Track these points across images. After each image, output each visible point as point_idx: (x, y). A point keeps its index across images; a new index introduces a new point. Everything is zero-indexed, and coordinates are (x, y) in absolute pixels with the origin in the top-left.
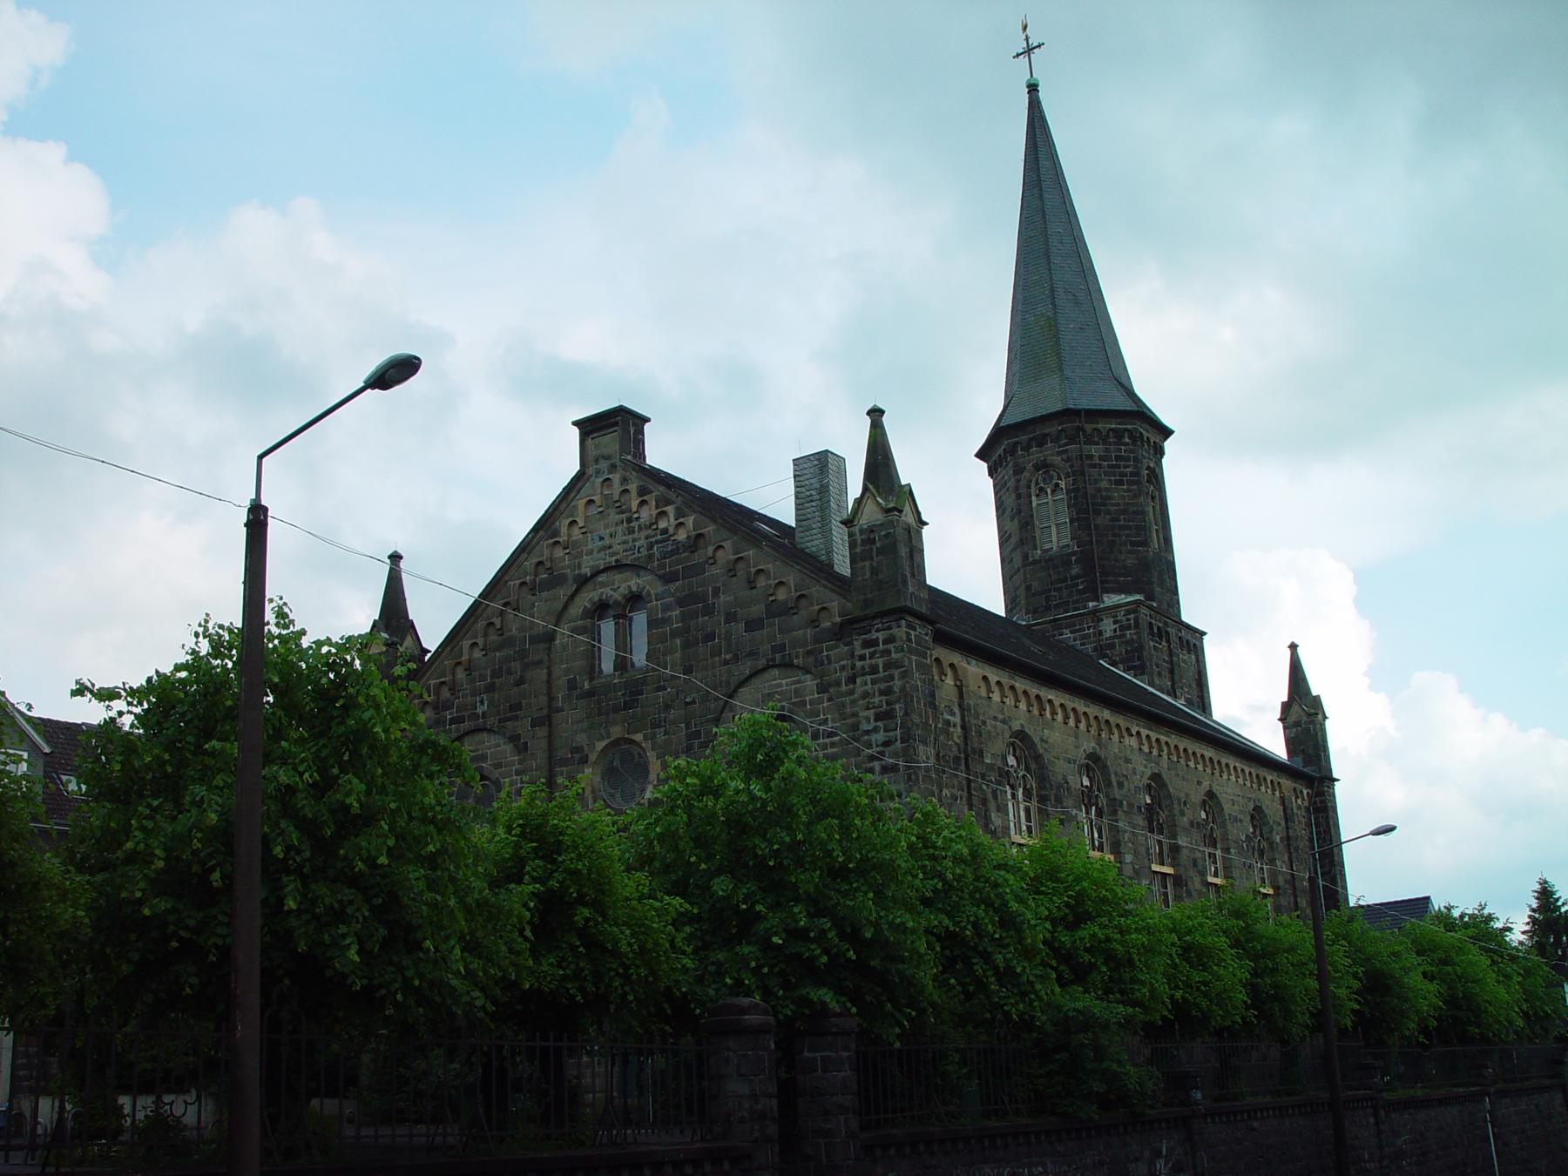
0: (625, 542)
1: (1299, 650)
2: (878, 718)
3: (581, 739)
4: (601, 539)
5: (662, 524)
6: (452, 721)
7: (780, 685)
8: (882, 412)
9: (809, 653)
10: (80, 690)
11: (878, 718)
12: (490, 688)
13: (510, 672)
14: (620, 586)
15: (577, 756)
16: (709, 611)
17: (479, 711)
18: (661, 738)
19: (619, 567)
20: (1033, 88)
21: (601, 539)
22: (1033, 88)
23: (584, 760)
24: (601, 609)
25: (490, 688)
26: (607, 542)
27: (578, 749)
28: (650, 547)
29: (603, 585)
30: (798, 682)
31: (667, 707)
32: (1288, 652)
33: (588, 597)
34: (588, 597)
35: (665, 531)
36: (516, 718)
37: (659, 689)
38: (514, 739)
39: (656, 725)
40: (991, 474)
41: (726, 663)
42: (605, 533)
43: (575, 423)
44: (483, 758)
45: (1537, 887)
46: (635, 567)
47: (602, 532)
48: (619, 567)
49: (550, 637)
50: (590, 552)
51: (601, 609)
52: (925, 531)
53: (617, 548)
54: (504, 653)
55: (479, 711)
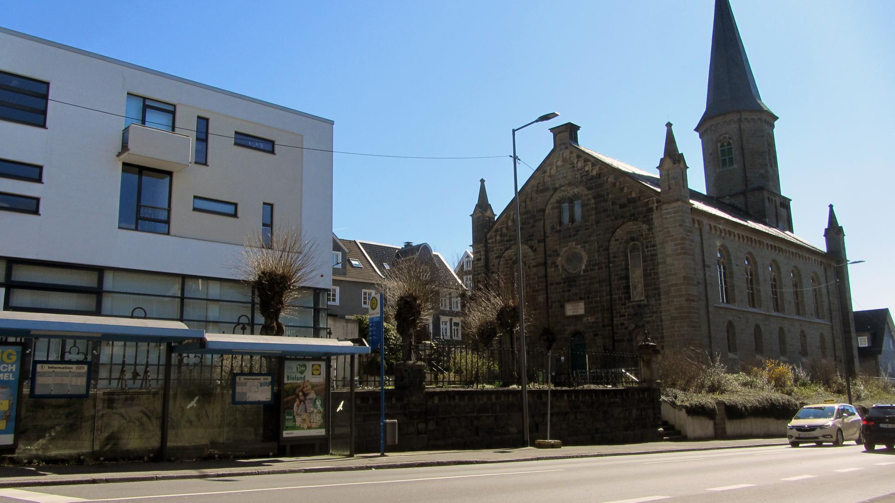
3: (557, 247)
6: (507, 241)
16: (606, 201)
18: (587, 247)
19: (570, 184)
28: (582, 177)
29: (564, 191)
39: (586, 242)
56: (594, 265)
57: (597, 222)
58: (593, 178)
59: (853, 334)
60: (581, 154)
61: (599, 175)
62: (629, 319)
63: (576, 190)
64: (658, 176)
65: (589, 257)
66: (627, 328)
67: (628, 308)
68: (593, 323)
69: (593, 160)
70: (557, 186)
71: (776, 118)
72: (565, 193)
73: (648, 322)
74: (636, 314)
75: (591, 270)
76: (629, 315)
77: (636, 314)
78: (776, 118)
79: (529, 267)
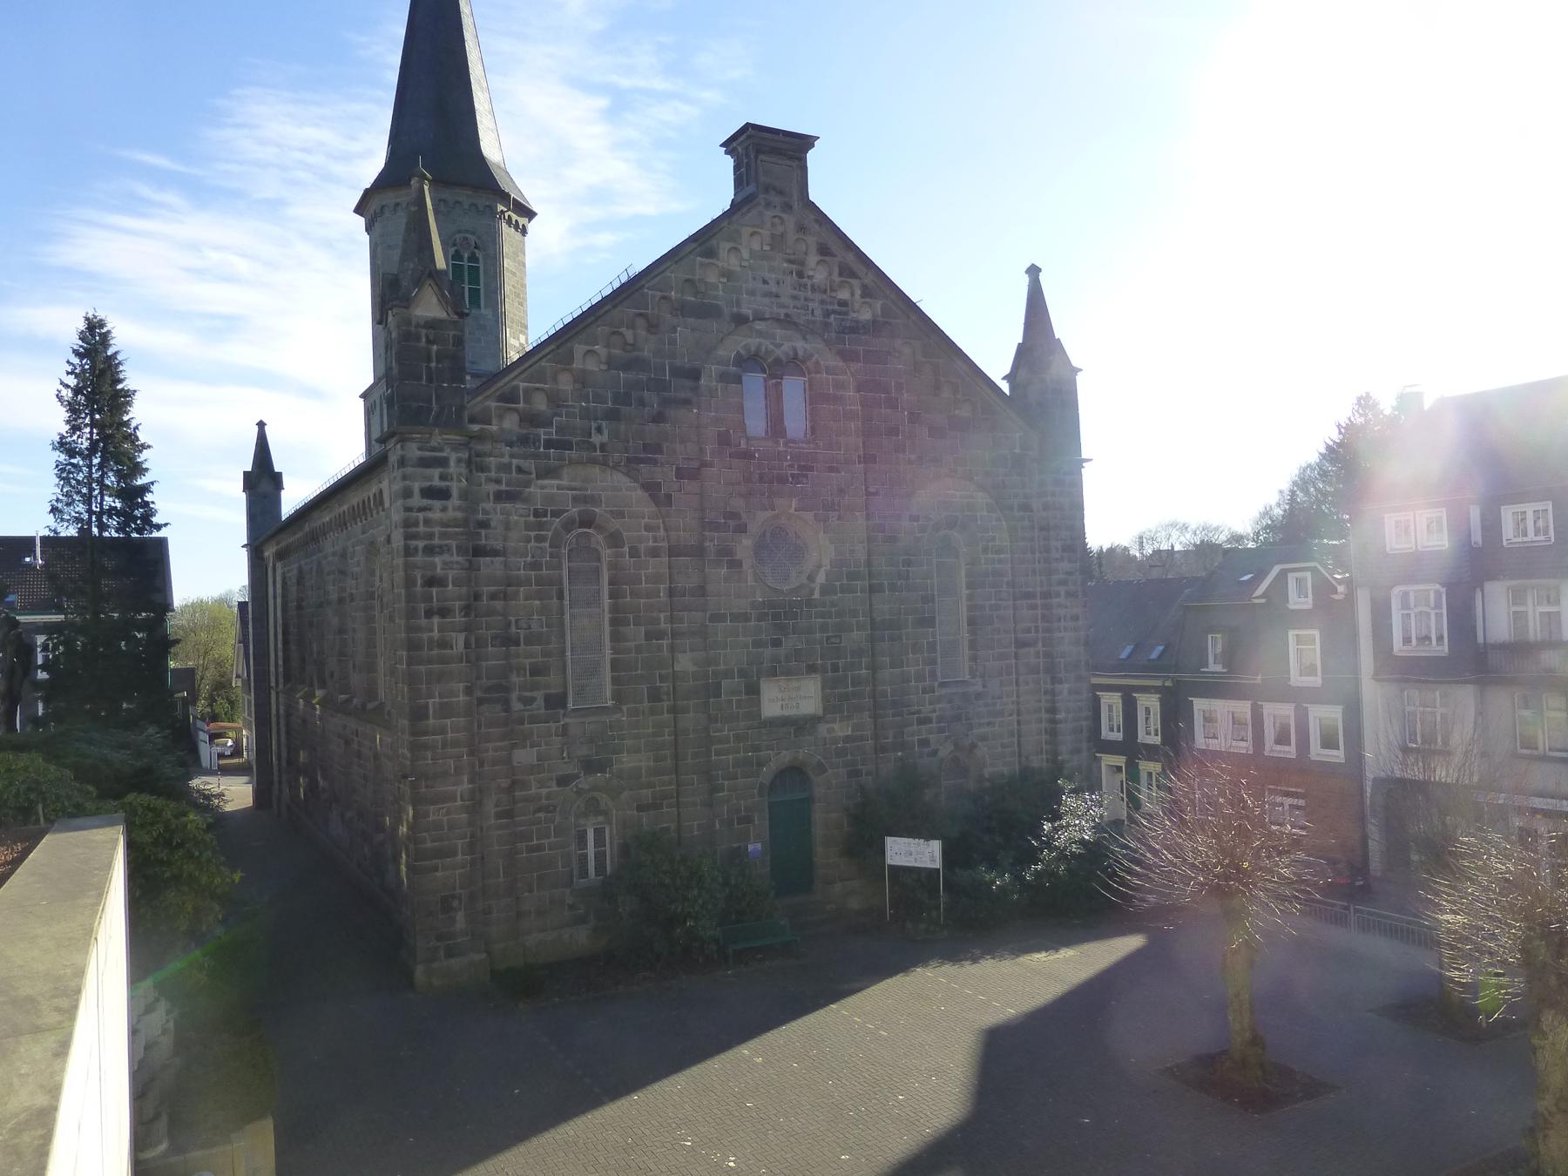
0: (795, 298)
1: (1042, 277)
2: (1064, 550)
3: (738, 504)
4: (765, 282)
5: (844, 295)
6: (549, 444)
8: (794, 147)
11: (1064, 550)
13: (642, 403)
15: (731, 523)
17: (596, 439)
19: (787, 322)
21: (765, 282)
23: (742, 529)
24: (750, 361)
25: (613, 416)
27: (734, 515)
28: (827, 314)
29: (760, 334)
31: (841, 491)
33: (742, 342)
34: (742, 342)
35: (843, 303)
36: (654, 462)
37: (831, 469)
38: (651, 488)
42: (771, 277)
44: (593, 500)
45: (82, 326)
47: (767, 275)
49: (695, 375)
50: (752, 293)
51: (750, 361)
52: (1080, 378)
53: (784, 300)
54: (631, 376)
55: (596, 439)
56: (853, 576)
57: (868, 459)
60: (835, 246)
62: (941, 730)
66: (935, 753)
68: (847, 739)
69: (869, 280)
70: (747, 311)
71: (804, 143)
72: (767, 344)
73: (984, 738)
78: (804, 143)
79: (634, 553)
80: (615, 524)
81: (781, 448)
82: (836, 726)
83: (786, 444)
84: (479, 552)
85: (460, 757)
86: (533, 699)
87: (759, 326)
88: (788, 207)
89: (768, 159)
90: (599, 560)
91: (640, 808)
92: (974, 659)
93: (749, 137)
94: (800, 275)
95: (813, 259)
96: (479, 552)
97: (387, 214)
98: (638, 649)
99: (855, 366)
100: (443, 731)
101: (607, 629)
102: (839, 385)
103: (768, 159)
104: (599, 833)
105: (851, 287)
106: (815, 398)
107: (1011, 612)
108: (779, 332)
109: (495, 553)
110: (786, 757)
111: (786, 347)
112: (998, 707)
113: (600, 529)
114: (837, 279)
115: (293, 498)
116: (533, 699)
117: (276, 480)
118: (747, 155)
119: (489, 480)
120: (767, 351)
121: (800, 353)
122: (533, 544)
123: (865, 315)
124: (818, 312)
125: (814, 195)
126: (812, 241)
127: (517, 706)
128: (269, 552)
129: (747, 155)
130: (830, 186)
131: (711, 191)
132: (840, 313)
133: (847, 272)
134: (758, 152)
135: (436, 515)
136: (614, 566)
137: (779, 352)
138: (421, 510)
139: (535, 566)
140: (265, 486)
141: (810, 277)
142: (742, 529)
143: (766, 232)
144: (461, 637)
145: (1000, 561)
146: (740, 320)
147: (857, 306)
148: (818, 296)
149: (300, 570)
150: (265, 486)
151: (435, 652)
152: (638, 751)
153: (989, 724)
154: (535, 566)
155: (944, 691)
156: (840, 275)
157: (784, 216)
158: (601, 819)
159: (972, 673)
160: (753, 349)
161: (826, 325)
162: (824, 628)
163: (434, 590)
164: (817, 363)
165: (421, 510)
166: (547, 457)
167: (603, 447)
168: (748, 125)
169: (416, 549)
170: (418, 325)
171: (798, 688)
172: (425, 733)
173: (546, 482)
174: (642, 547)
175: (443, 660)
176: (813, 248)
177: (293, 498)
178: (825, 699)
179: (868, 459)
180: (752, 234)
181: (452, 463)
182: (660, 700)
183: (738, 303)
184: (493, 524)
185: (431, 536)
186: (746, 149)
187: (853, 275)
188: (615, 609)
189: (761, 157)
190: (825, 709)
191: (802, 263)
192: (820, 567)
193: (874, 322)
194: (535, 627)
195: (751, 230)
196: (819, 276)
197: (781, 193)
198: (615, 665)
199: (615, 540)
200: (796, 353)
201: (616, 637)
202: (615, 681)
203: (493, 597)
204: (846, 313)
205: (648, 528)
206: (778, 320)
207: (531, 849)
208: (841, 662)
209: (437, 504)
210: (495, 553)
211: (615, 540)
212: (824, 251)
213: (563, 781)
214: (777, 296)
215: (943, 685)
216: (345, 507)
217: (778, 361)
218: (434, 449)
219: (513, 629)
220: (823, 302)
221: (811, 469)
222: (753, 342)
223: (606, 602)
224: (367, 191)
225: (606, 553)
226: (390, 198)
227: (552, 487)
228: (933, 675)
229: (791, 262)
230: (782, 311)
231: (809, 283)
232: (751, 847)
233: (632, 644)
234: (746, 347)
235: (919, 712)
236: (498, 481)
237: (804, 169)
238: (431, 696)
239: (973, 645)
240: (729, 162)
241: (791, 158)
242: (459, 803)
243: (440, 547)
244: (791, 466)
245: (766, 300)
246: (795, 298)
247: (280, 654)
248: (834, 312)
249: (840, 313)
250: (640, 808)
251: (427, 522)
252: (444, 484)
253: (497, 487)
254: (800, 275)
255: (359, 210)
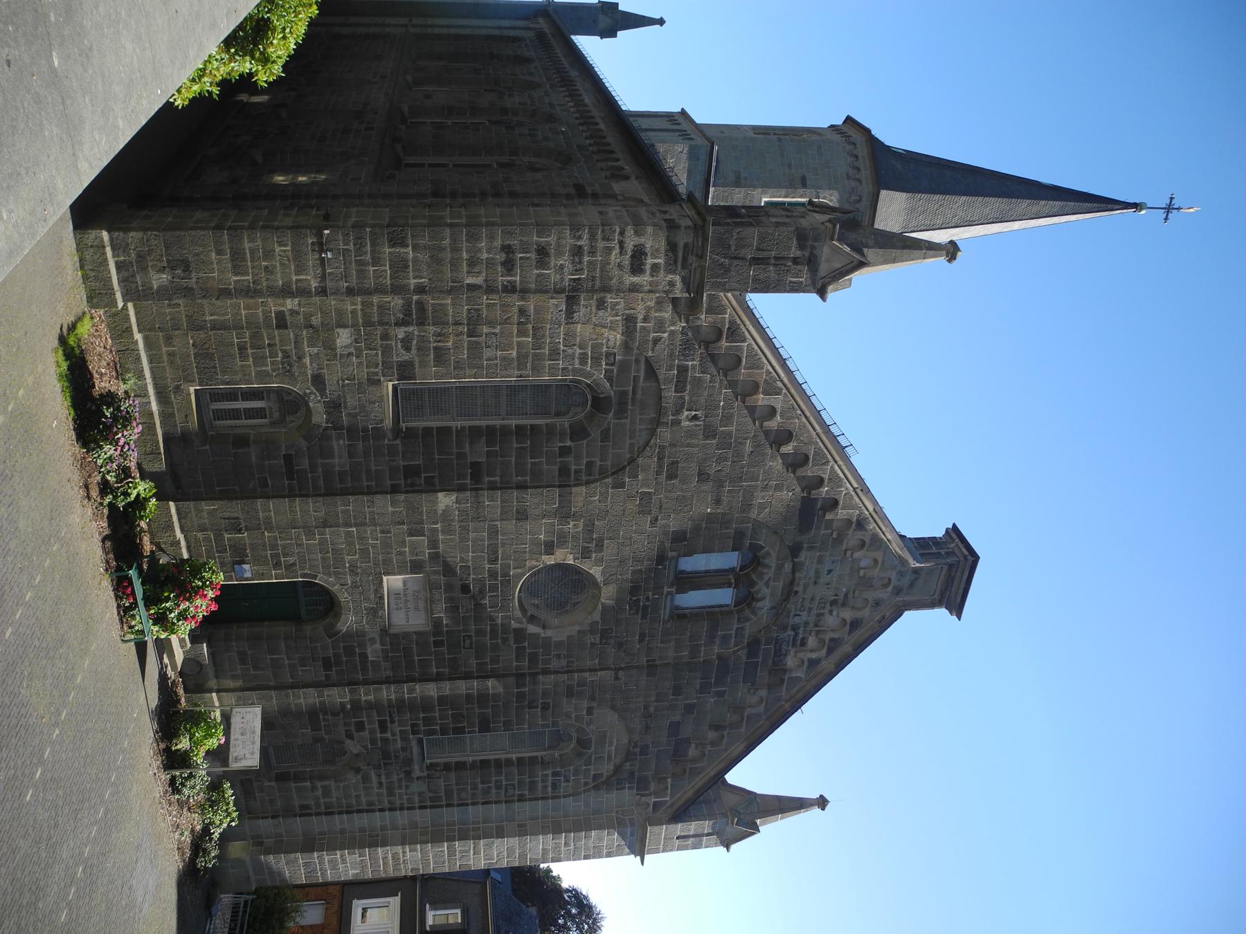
1: (816, 811)
3: (610, 550)
5: (812, 642)
6: (683, 370)
7: (611, 744)
8: (952, 596)
9: (632, 774)
10: (951, 251)
12: (709, 432)
14: (767, 593)
16: (704, 689)
18: (589, 639)
19: (789, 591)
20: (1136, 206)
21: (830, 571)
22: (1136, 206)
26: (824, 579)
27: (600, 547)
28: (795, 628)
29: (780, 567)
30: (609, 758)
31: (620, 645)
32: (658, 17)
35: (803, 643)
37: (642, 636)
39: (605, 634)
40: (832, 126)
41: (646, 707)
43: (954, 525)
46: (779, 610)
48: (789, 591)
56: (533, 659)
57: (651, 668)
58: (779, 654)
59: (274, 699)
60: (859, 634)
61: (778, 671)
62: (373, 741)
63: (765, 605)
64: (732, 777)
65: (559, 645)
66: (350, 737)
67: (405, 739)
68: (364, 656)
69: (827, 665)
70: (803, 556)
71: (957, 609)
72: (769, 574)
73: (366, 779)
74: (386, 755)
75: (520, 652)
76: (385, 740)
77: (386, 755)
78: (957, 609)
79: (564, 451)
80: (595, 434)
81: (666, 589)
82: (378, 646)
83: (669, 593)
84: (572, 301)
85: (346, 277)
86: (408, 349)
87: (788, 567)
88: (898, 591)
89: (946, 571)
90: (558, 414)
91: (288, 458)
92: (447, 767)
93: (965, 558)
94: (833, 603)
95: (847, 615)
96: (572, 301)
97: (848, 147)
98: (461, 456)
99: (743, 654)
100: (376, 261)
101: (483, 423)
102: (725, 639)
103: (946, 571)
104: (259, 413)
105: (819, 650)
106: (713, 615)
107: (493, 799)
108: (780, 584)
109: (570, 313)
110: (344, 597)
111: (766, 591)
112: (397, 791)
113: (590, 417)
114: (827, 637)
115: (588, 45)
116: (408, 349)
117: (609, 33)
118: (948, 554)
119: (648, 309)
120: (762, 574)
121: (759, 604)
122: (578, 351)
123: (790, 661)
124: (797, 620)
125: (910, 617)
126: (866, 613)
127: (401, 333)
128: (542, 23)
129: (948, 554)
130: (919, 627)
131: (912, 513)
132: (794, 640)
133: (834, 645)
134: (951, 566)
135: (614, 257)
136: (551, 429)
137: (761, 584)
138: (621, 243)
139: (554, 354)
140: (604, 21)
141: (831, 612)
142: (585, 554)
143: (876, 572)
144: (479, 280)
145: (545, 787)
146: (795, 550)
147: (801, 655)
148: (812, 620)
149: (528, 60)
150: (604, 21)
151: (465, 256)
152: (351, 455)
153: (380, 784)
154: (554, 354)
155: (414, 743)
156: (832, 640)
157: (890, 588)
158: (276, 415)
159: (431, 767)
160: (766, 561)
161: (785, 628)
162: (480, 633)
163: (533, 256)
164: (747, 620)
165: (621, 243)
166: (671, 368)
167: (677, 423)
168: (976, 558)
169: (580, 238)
170: (813, 248)
171: (417, 609)
172: (373, 244)
173: (643, 366)
174: (570, 459)
175: (455, 264)
176: (858, 615)
177: (588, 45)
178: (406, 635)
179: (651, 668)
180: (876, 561)
181: (656, 261)
182: (406, 478)
183: (811, 548)
184: (601, 313)
185: (592, 252)
186: (953, 553)
187: (830, 651)
188: (505, 431)
189: (946, 567)
190: (396, 636)
191: (844, 605)
192: (544, 627)
193: (785, 671)
194: (488, 353)
195: (880, 560)
196: (831, 621)
197: (912, 585)
198: (444, 432)
199: (578, 432)
200: (758, 600)
201: (475, 433)
202: (428, 431)
203: (522, 312)
204: (794, 645)
205: (590, 465)
206: (792, 583)
207: (242, 348)
208: (445, 649)
209: (626, 260)
210: (570, 313)
211: (578, 432)
212: (855, 624)
213: (318, 380)
214: (815, 583)
215: (420, 741)
216: (602, 126)
217: (752, 584)
218: (685, 259)
219: (485, 330)
220: (806, 624)
221: (644, 617)
222: (772, 562)
223: (513, 422)
224: (868, 131)
225: (565, 422)
226: (863, 151)
227: (638, 371)
228: (432, 732)
229: (846, 595)
230: (800, 589)
231: (826, 611)
232: (246, 567)
233: (467, 449)
234: (768, 554)
235: (392, 722)
236: (645, 319)
237: (932, 605)
238: (415, 248)
239: (460, 766)
240: (939, 533)
241: (942, 594)
242: (294, 278)
243: (580, 262)
244: (648, 599)
245: (812, 574)
246: (812, 599)
247: (444, 31)
248: (797, 634)
249: (794, 640)
250: (288, 458)
251: (610, 249)
252: (648, 267)
253: (641, 317)
254: (833, 603)
255: (849, 120)
